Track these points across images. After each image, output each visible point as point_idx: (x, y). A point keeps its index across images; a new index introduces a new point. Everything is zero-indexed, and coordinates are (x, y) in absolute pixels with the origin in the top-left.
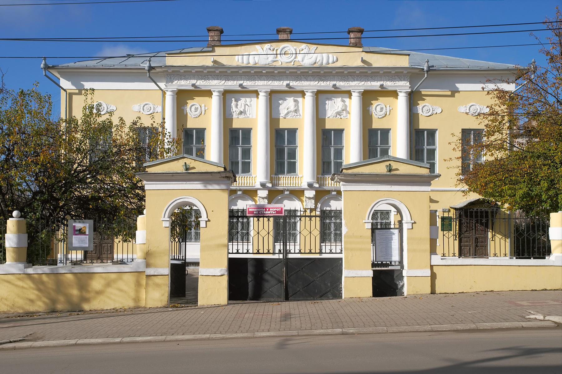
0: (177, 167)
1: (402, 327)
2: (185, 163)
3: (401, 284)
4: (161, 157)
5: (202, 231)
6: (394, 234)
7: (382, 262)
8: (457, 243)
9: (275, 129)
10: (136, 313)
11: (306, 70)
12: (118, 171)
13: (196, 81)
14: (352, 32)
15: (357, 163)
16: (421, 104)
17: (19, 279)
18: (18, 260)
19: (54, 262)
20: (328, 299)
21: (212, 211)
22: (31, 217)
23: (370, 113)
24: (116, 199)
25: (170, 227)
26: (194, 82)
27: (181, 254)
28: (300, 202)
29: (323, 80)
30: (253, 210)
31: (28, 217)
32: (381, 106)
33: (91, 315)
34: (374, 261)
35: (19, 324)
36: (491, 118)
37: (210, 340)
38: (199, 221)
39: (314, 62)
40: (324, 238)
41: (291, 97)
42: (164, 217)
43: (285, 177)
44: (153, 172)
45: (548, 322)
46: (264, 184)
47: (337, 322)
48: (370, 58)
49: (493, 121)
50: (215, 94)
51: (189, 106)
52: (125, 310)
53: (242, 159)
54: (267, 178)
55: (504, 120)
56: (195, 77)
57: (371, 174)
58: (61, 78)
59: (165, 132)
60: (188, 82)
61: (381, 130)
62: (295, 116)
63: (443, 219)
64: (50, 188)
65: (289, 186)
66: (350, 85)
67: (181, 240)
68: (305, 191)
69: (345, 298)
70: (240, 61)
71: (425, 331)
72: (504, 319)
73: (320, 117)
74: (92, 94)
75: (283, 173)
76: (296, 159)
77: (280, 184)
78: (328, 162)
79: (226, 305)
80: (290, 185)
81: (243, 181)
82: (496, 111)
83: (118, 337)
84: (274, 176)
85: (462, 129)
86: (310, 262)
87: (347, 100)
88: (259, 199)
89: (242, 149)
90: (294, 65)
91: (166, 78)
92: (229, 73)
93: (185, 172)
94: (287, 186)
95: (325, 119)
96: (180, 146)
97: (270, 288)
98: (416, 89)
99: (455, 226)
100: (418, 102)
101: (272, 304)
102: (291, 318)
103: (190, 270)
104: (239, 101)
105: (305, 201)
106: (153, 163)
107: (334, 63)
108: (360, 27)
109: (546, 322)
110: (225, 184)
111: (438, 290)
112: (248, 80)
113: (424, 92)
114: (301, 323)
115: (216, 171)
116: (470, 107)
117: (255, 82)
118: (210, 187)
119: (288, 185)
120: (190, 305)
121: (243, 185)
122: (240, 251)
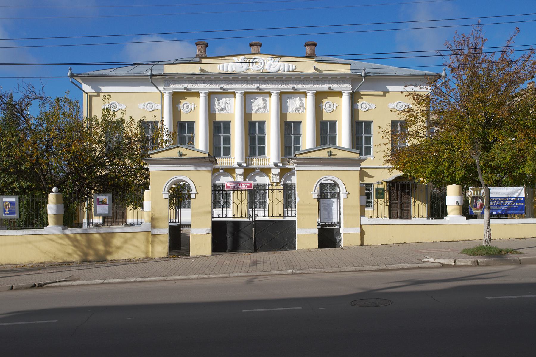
0: (173, 154)
1: (335, 268)
2: (179, 151)
3: (339, 239)
4: (161, 146)
5: (192, 201)
6: (334, 202)
7: (332, 223)
8: (387, 208)
9: (249, 122)
10: (145, 262)
11: (272, 76)
12: (129, 157)
14: (308, 45)
15: (312, 148)
16: (360, 102)
17: (61, 238)
18: (57, 223)
19: (80, 225)
20: (286, 251)
22: (65, 192)
24: (129, 178)
25: (169, 198)
26: (185, 85)
27: (177, 219)
28: (268, 178)
29: (285, 84)
30: (230, 185)
31: (64, 192)
32: (330, 104)
33: (112, 264)
34: (320, 222)
35: (60, 270)
36: (409, 114)
38: (190, 194)
39: (278, 70)
41: (260, 97)
42: (164, 191)
43: (256, 158)
44: (156, 158)
45: (437, 263)
46: (240, 164)
47: (289, 266)
49: (410, 116)
51: (182, 104)
52: (136, 260)
53: (223, 145)
54: (242, 159)
55: (418, 116)
57: (317, 158)
58: (83, 84)
59: (164, 128)
60: (181, 86)
61: (330, 122)
62: (264, 112)
63: (377, 189)
64: (79, 170)
65: (260, 165)
66: (306, 87)
67: (177, 208)
68: (272, 169)
69: (298, 249)
70: (221, 69)
71: (351, 271)
72: (407, 262)
74: (109, 99)
75: (255, 155)
76: (264, 145)
77: (253, 164)
79: (211, 256)
80: (261, 164)
81: (226, 162)
82: (412, 109)
83: (133, 278)
84: (248, 158)
85: (391, 121)
86: (272, 223)
87: (304, 99)
88: (237, 176)
89: (223, 137)
92: (213, 79)
94: (258, 165)
95: (287, 113)
96: (175, 138)
97: (243, 243)
98: (356, 91)
99: (386, 195)
100: (358, 100)
101: (244, 255)
102: (257, 264)
103: (184, 230)
104: (221, 100)
105: (272, 177)
106: (155, 151)
108: (314, 42)
109: (435, 263)
110: (209, 166)
112: (228, 84)
113: (362, 92)
114: (264, 267)
115: (202, 157)
116: (398, 104)
117: (233, 85)
118: (199, 169)
119: (259, 164)
120: (185, 256)
121: (224, 165)
122: (221, 216)
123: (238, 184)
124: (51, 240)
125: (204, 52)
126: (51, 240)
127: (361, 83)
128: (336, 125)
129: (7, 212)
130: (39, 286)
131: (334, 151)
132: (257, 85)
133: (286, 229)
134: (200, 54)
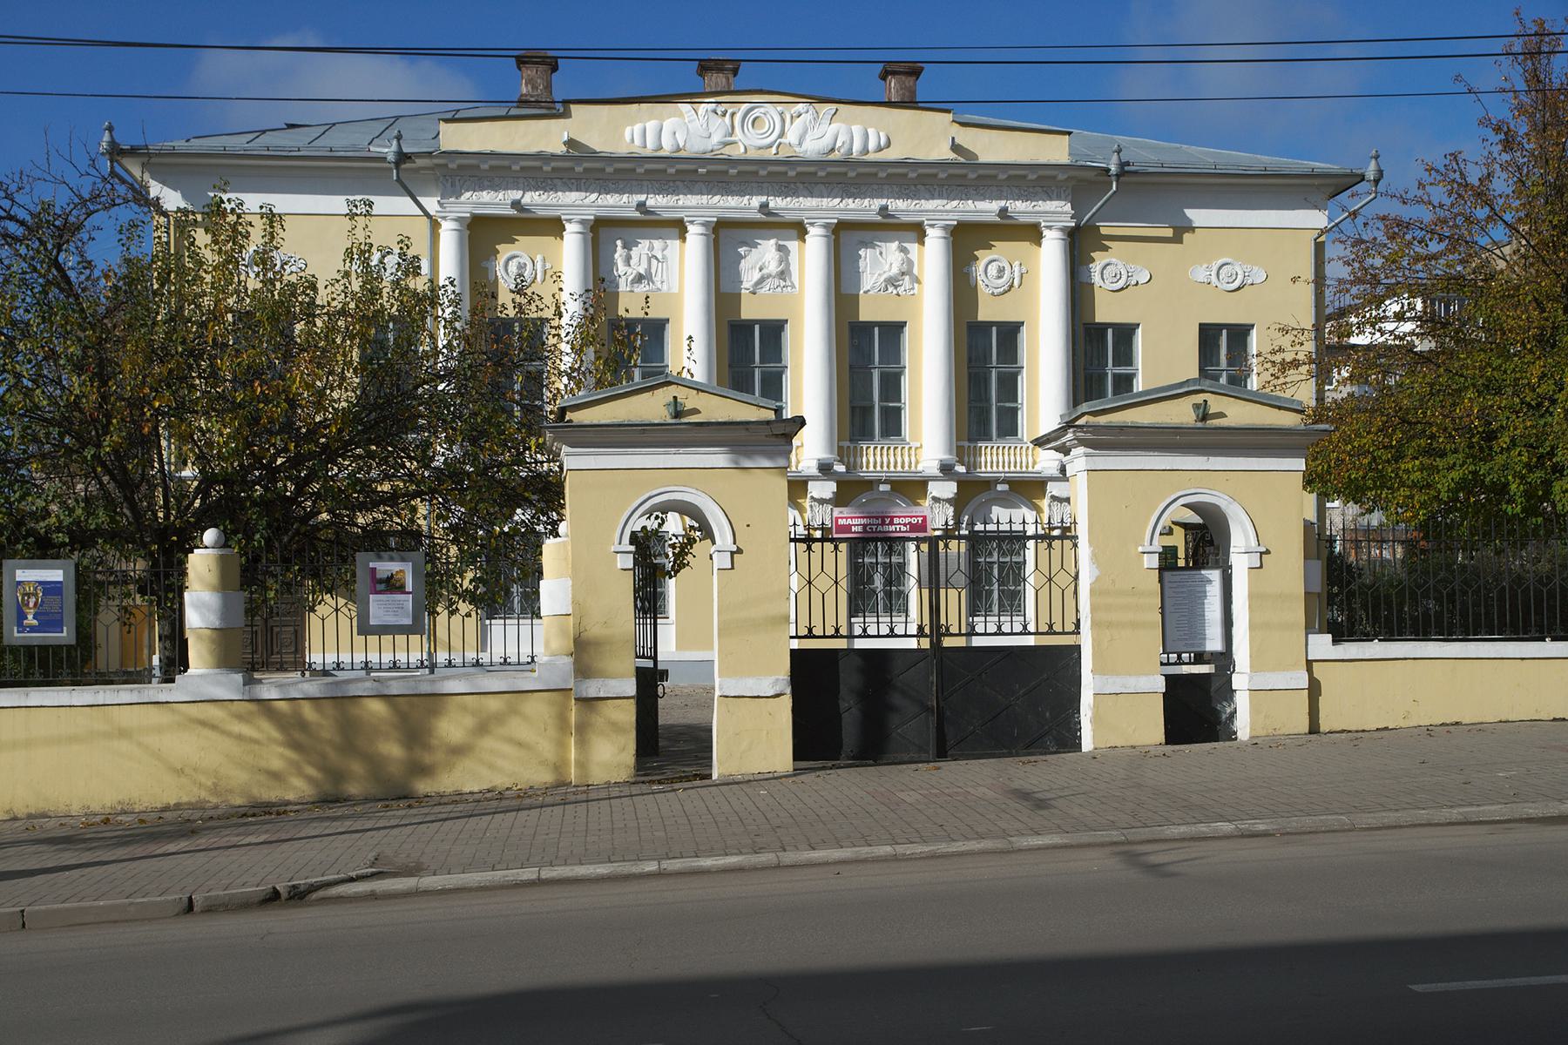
2: (675, 398)
3: (1228, 710)
6: (1210, 581)
11: (812, 169)
13: (521, 192)
14: (894, 73)
16: (1100, 259)
17: (240, 717)
20: (1045, 754)
21: (748, 526)
23: (972, 283)
26: (516, 195)
30: (849, 521)
37: (900, 860)
39: (830, 147)
40: (859, 601)
44: (587, 422)
48: (968, 138)
50: (572, 229)
51: (501, 259)
52: (501, 796)
56: (518, 183)
60: (501, 195)
61: (999, 324)
62: (779, 289)
70: (637, 142)
73: (843, 291)
78: (864, 408)
85: (1200, 324)
87: (913, 248)
90: (777, 153)
91: (440, 184)
93: (673, 421)
98: (1088, 221)
106: (613, 390)
107: (881, 150)
111: (1324, 726)
123: (877, 518)
124: (203, 723)
125: (545, 88)
126: (203, 723)
127: (1099, 204)
128: (1020, 336)
129: (31, 620)
130: (291, 898)
131: (1216, 404)
132: (759, 197)
133: (1045, 676)
134: (532, 96)
